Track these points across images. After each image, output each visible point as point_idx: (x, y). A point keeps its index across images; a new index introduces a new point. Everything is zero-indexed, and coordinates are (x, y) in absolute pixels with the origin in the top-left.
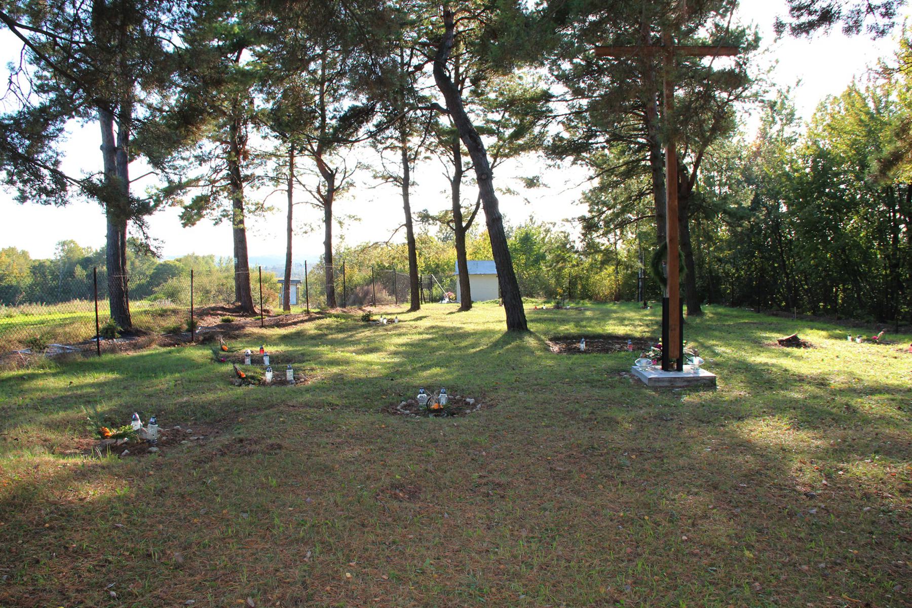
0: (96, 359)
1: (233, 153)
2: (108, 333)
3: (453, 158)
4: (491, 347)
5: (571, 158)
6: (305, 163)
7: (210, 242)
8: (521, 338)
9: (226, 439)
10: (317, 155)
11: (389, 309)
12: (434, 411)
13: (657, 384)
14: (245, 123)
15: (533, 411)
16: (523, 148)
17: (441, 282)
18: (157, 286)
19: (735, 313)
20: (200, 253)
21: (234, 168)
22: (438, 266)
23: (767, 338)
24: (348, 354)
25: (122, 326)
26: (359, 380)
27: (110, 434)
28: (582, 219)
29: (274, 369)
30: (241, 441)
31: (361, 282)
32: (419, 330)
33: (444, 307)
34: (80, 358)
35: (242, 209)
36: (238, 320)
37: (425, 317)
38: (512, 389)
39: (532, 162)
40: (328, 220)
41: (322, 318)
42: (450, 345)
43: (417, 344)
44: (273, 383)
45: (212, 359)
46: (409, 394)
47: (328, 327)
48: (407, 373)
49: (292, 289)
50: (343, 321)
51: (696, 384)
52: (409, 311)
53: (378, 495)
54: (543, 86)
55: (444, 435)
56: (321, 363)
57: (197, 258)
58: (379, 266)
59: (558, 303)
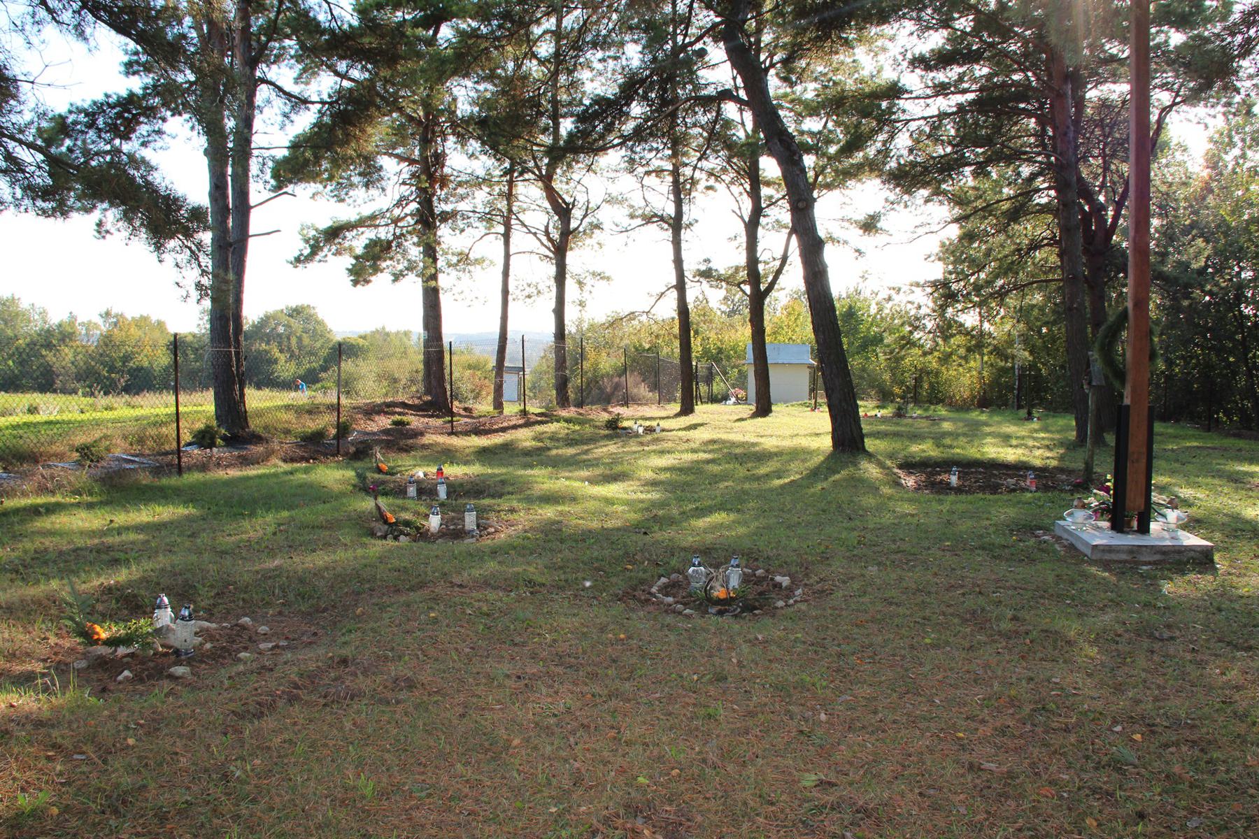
1: (424, 177)
2: (204, 438)
3: (748, 187)
4: (808, 477)
5: (924, 192)
6: (529, 192)
8: (855, 465)
9: (312, 658)
10: (546, 181)
11: (648, 411)
12: (719, 602)
13: (1107, 557)
15: (901, 610)
17: (725, 373)
19: (1170, 431)
20: (392, 328)
22: (720, 351)
24: (577, 484)
25: (233, 428)
27: (104, 635)
28: (935, 284)
30: (344, 661)
32: (692, 445)
33: (730, 410)
34: (145, 479)
35: (435, 260)
36: (415, 421)
37: (702, 425)
38: (853, 559)
39: (869, 194)
40: (560, 278)
42: (741, 472)
43: (689, 469)
45: (354, 486)
46: (674, 562)
47: (554, 438)
48: (671, 521)
50: (577, 427)
51: (1179, 561)
52: (677, 415)
54: (889, 75)
56: (530, 500)
57: (388, 334)
58: (637, 349)
59: (899, 409)
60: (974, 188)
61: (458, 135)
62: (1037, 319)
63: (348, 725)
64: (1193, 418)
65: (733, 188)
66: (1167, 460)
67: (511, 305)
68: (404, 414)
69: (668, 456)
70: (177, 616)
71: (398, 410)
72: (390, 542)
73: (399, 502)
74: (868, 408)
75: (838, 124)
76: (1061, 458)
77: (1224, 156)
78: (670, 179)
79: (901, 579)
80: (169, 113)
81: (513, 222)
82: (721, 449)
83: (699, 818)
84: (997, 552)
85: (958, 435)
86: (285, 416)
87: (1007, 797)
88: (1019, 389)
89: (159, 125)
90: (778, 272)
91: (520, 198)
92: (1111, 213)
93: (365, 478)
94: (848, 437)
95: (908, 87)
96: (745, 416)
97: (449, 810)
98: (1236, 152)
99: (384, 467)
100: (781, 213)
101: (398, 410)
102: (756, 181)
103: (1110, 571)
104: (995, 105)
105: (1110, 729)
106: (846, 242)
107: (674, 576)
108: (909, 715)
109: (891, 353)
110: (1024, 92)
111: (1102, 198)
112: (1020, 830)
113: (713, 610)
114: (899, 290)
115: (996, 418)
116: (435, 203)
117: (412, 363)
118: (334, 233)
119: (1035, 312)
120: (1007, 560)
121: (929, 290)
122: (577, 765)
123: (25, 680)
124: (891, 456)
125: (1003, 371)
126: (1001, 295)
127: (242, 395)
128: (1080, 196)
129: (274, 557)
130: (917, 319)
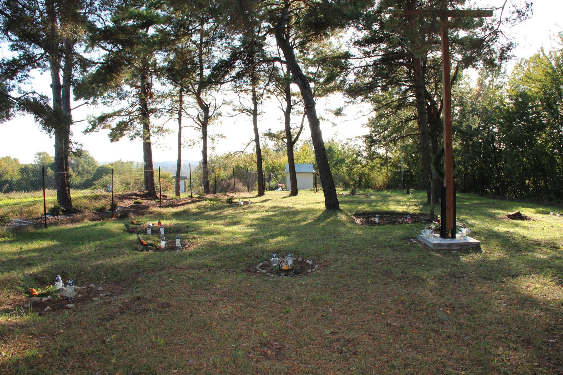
0: (44, 230)
1: (143, 94)
2: (54, 211)
3: (285, 97)
4: (316, 221)
5: (361, 98)
6: (189, 100)
7: (129, 151)
8: (336, 215)
9: (126, 297)
10: (197, 95)
11: (243, 195)
12: (285, 271)
13: (439, 248)
14: (151, 75)
15: (358, 271)
16: (332, 90)
18: (97, 180)
19: (467, 197)
20: (124, 160)
21: (144, 104)
22: (273, 167)
23: (498, 214)
24: (219, 226)
25: (66, 207)
26: (227, 247)
27: (37, 293)
28: (367, 137)
29: (166, 238)
30: (139, 299)
31: (225, 177)
34: (31, 230)
35: (149, 130)
36: (144, 202)
37: (268, 200)
39: (337, 99)
41: (201, 201)
42: (288, 219)
44: (166, 249)
45: (124, 230)
46: (265, 256)
47: (205, 207)
48: (261, 240)
49: (181, 182)
50: (215, 203)
53: (250, 353)
54: (344, 49)
55: (297, 293)
57: (122, 163)
58: (237, 168)
59: (353, 191)
60: (382, 96)
61: (157, 75)
62: (410, 151)
63: (147, 321)
64: (476, 191)
65: (278, 97)
66: (465, 209)
67: (182, 149)
68: (137, 199)
69: (255, 214)
70: (65, 284)
71: (134, 197)
72: (145, 253)
73: (146, 236)
74: (340, 191)
75: (323, 69)
76: (421, 210)
77: (484, 80)
78: (252, 94)
79: (357, 259)
80: (31, 67)
81: (182, 113)
82: (278, 210)
83: (288, 346)
84: (395, 248)
85: (378, 201)
86: (84, 201)
87: (401, 334)
88: (403, 181)
89: (27, 73)
90: (299, 133)
91: (186, 102)
92: (439, 105)
93: (129, 226)
94: (332, 203)
95: (353, 54)
96: (286, 196)
97: (193, 348)
98: (489, 78)
99: (135, 222)
100: (300, 108)
101: (134, 197)
102: (288, 94)
103: (440, 253)
104: (388, 60)
105: (438, 309)
106: (328, 120)
107: (265, 262)
108: (363, 308)
109: (348, 167)
110: (401, 55)
111: (435, 99)
112: (406, 344)
113: (282, 274)
114: (351, 140)
115: (394, 194)
116: (148, 105)
117: (136, 176)
118: (102, 119)
119: (409, 148)
120: (400, 251)
121: (364, 139)
122: (239, 331)
123: (7, 311)
124: (351, 211)
125: (396, 173)
126: (395, 141)
127: (69, 192)
128: (426, 98)
129: (98, 260)
130: (359, 152)
